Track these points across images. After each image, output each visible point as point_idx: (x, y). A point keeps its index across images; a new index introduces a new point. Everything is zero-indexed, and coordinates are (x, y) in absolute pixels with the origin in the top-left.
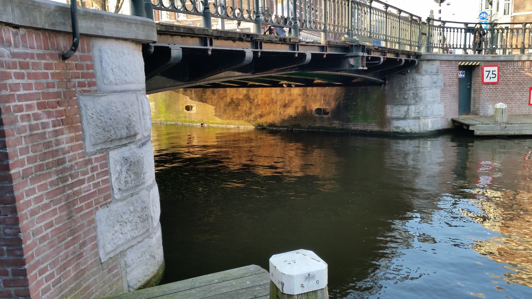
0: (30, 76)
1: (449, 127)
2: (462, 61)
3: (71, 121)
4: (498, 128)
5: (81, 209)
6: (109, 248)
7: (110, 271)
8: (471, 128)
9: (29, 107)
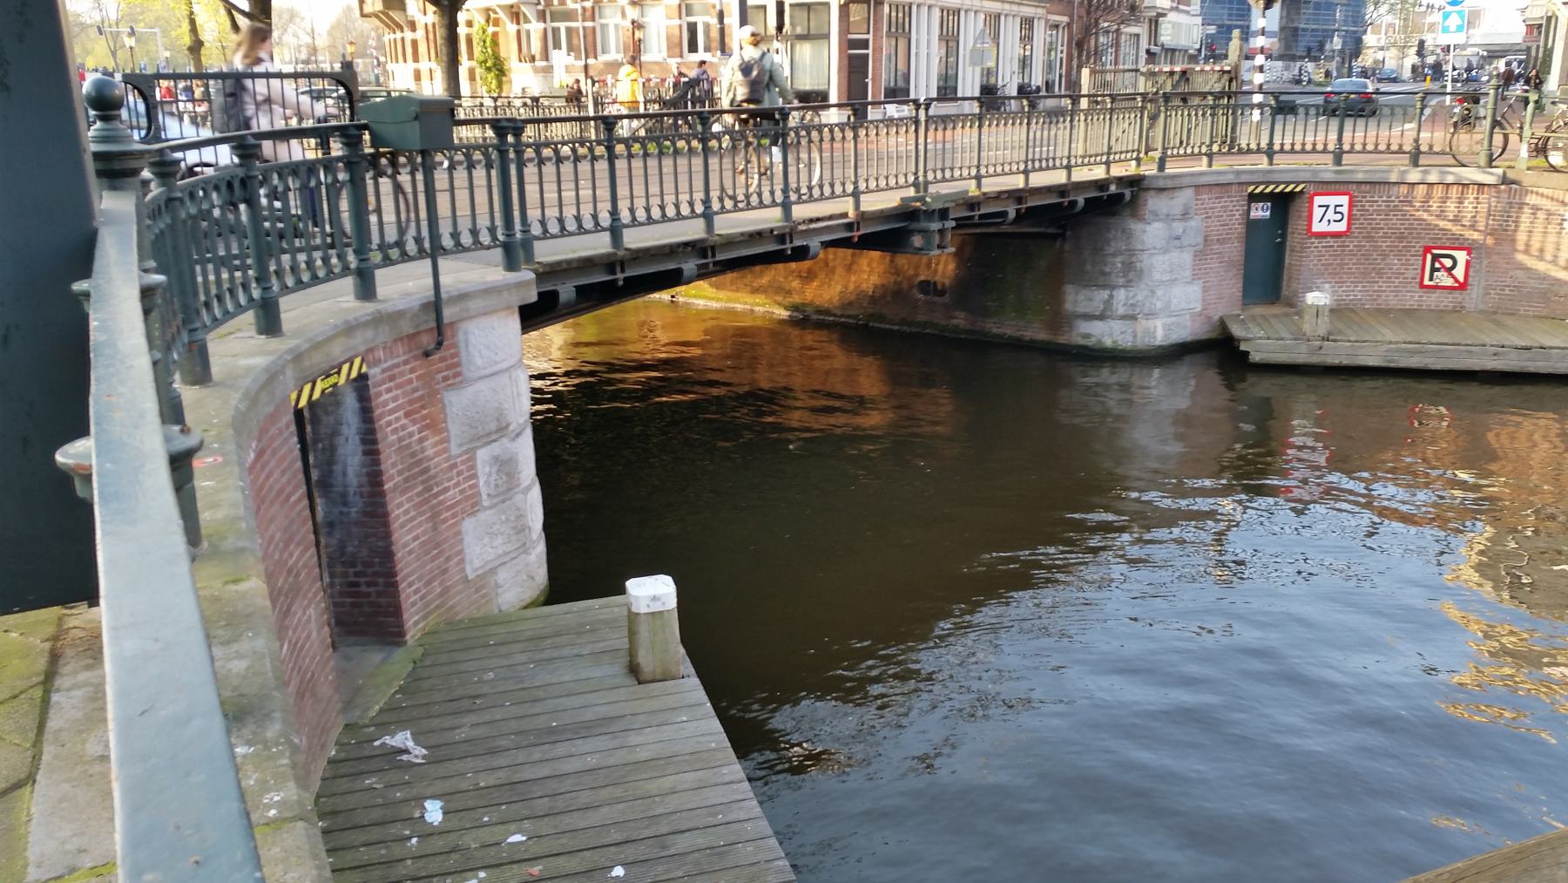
0: (398, 387)
1: (1213, 335)
2: (1258, 184)
3: (435, 425)
4: (1304, 348)
5: (445, 521)
6: (477, 564)
7: (477, 591)
8: (1243, 347)
9: (397, 419)
